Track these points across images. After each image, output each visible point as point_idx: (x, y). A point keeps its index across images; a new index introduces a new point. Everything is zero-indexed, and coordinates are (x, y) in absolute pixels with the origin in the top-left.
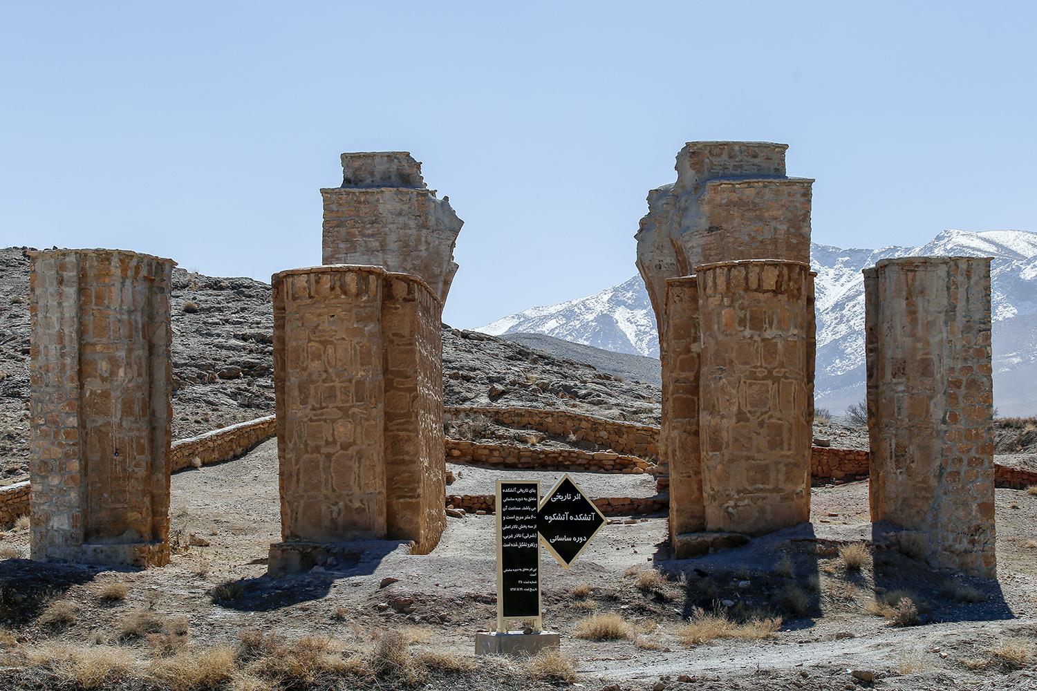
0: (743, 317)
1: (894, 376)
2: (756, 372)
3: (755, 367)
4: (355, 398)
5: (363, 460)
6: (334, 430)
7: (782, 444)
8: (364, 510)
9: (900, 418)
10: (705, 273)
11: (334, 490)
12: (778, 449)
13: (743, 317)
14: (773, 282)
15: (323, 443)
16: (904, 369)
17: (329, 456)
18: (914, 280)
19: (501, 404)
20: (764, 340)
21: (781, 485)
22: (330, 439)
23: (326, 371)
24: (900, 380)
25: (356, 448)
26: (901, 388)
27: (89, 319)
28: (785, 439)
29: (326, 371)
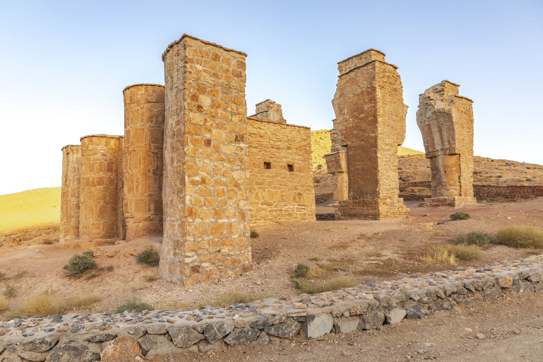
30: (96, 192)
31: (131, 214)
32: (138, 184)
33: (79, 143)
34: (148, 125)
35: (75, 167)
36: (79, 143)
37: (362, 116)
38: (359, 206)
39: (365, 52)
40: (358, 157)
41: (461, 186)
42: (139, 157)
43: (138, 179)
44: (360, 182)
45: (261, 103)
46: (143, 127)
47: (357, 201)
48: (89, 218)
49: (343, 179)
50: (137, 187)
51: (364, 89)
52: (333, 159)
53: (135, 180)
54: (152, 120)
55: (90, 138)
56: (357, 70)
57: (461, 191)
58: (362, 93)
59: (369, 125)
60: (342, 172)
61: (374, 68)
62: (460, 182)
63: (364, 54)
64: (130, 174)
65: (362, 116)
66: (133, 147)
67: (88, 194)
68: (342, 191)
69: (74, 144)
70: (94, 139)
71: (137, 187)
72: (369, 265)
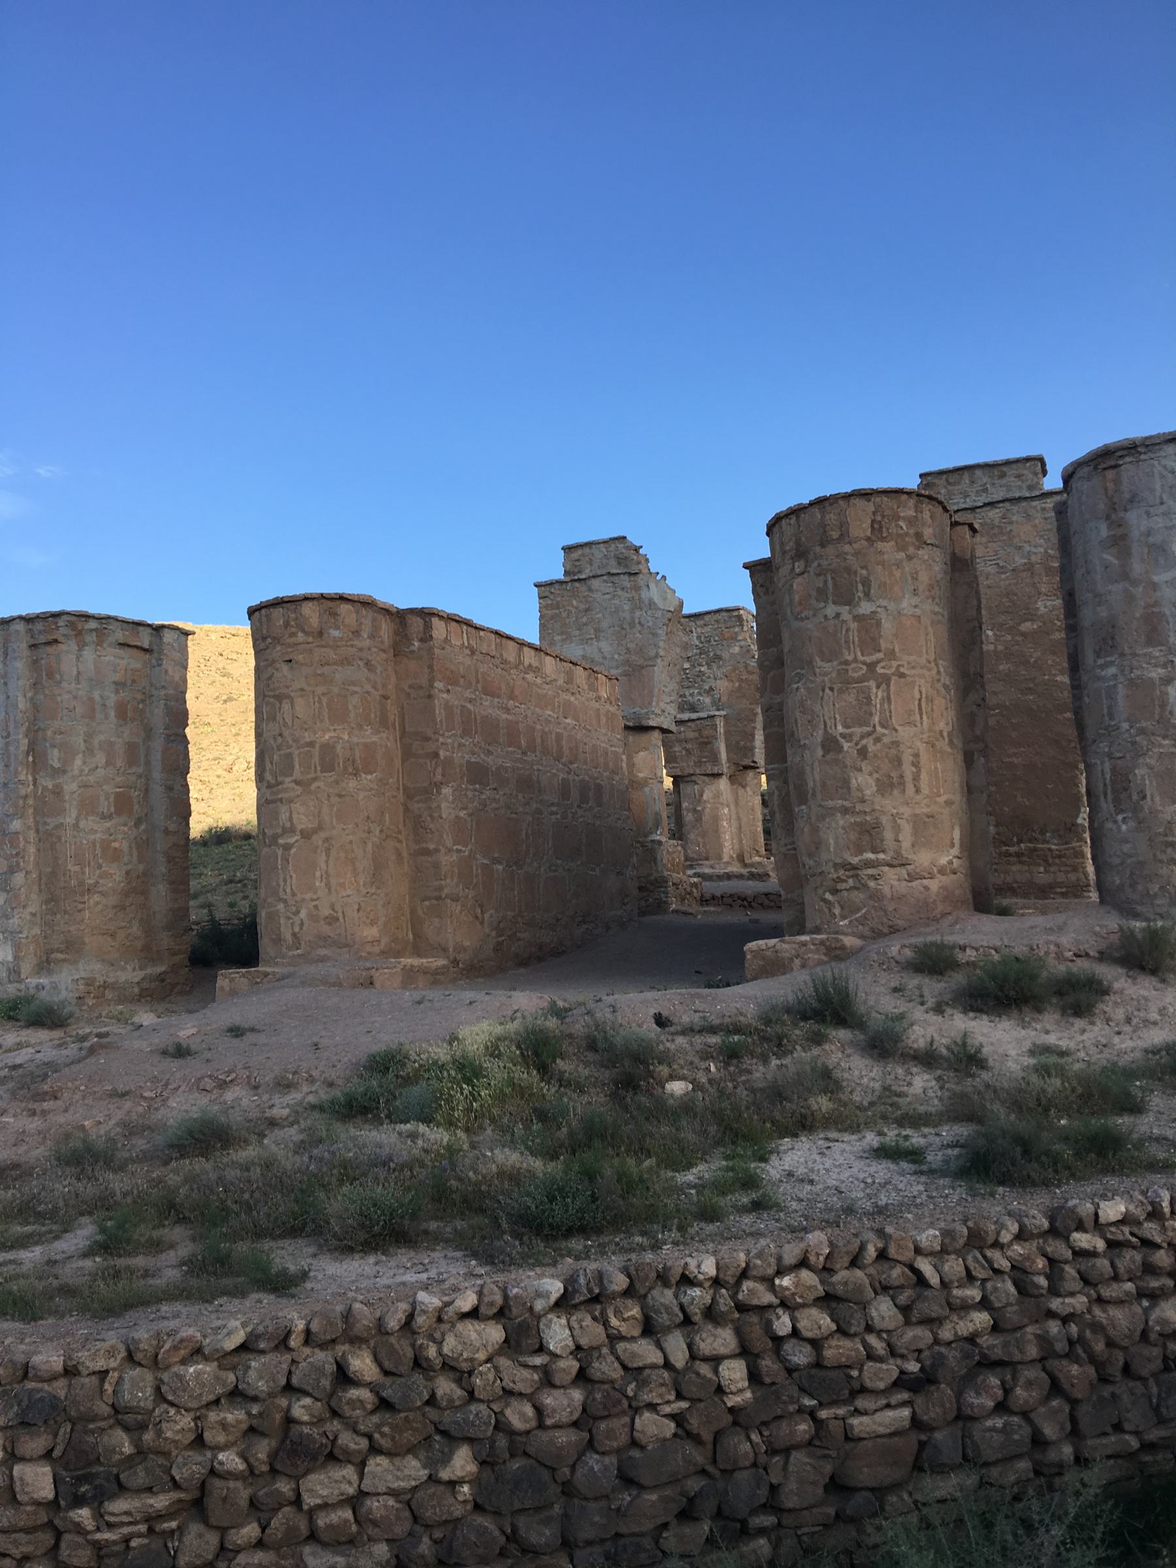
0: (821, 585)
1: (1098, 654)
2: (847, 671)
3: (846, 663)
4: (319, 768)
5: (333, 853)
6: (291, 813)
7: (902, 783)
8: (337, 919)
9: (1113, 723)
10: (798, 517)
11: (294, 895)
12: (896, 792)
13: (821, 585)
14: (867, 524)
15: (279, 831)
16: (1113, 638)
17: (287, 848)
18: (1117, 481)
19: (760, 756)
20: (857, 618)
21: (907, 853)
22: (288, 825)
23: (281, 735)
24: (1108, 659)
25: (323, 835)
26: (1112, 670)
27: (707, 618)
28: (908, 776)
29: (281, 735)
30: (362, 795)
31: (898, 853)
32: (919, 771)
35: (91, 700)
37: (1026, 626)
38: (1021, 863)
39: (1017, 461)
40: (1014, 734)
42: (917, 696)
43: (917, 755)
44: (1019, 799)
45: (589, 544)
46: (918, 612)
47: (1012, 849)
48: (342, 885)
49: (718, 795)
50: (916, 778)
52: (691, 735)
53: (907, 758)
54: (933, 593)
55: (330, 604)
56: (1007, 504)
58: (1029, 567)
59: (1054, 653)
60: (719, 775)
63: (1014, 466)
64: (886, 740)
65: (1026, 626)
66: (895, 664)
67: (334, 799)
68: (717, 831)
69: (92, 610)
70: (344, 608)
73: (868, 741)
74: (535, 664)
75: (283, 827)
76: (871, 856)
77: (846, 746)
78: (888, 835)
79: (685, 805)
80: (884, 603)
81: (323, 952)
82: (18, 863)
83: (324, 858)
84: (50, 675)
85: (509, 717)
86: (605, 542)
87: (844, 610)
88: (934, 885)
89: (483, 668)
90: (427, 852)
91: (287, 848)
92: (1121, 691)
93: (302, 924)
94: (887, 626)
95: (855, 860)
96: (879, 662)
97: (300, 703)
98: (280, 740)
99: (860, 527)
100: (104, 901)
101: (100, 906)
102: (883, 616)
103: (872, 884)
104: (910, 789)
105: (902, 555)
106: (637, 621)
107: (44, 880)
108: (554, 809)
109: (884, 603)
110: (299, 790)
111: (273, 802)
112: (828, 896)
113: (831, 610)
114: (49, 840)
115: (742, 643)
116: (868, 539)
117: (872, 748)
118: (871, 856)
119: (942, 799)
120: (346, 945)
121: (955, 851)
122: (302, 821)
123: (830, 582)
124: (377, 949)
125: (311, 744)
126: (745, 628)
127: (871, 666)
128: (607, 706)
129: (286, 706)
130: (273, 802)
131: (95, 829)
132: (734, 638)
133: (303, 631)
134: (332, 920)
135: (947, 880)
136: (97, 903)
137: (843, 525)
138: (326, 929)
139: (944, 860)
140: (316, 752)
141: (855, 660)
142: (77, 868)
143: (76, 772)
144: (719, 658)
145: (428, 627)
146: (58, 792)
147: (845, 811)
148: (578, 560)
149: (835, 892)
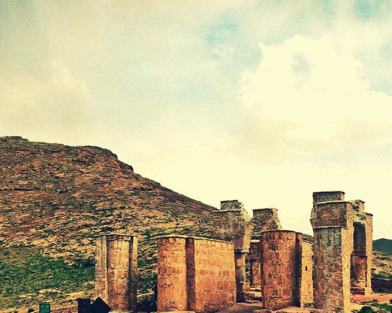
11: (166, 297)
17: (165, 288)
20: (276, 253)
21: (282, 296)
22: (165, 283)
23: (164, 265)
25: (172, 286)
28: (283, 282)
29: (164, 265)
31: (280, 296)
33: (218, 206)
34: (289, 251)
36: (218, 206)
41: (366, 280)
42: (285, 267)
45: (228, 201)
46: (286, 252)
50: (284, 283)
51: (338, 218)
53: (283, 279)
57: (366, 284)
61: (345, 206)
62: (366, 277)
71: (284, 283)
72: (224, 209)
73: (276, 276)
74: (214, 244)
75: (164, 284)
76: (276, 296)
77: (272, 276)
78: (279, 292)
79: (253, 268)
80: (280, 251)
81: (172, 309)
82: (105, 288)
83: (172, 290)
84: (112, 247)
85: (209, 258)
86: (232, 201)
87: (273, 251)
88: (286, 301)
89: (203, 248)
90: (191, 289)
91: (165, 288)
92: (317, 270)
93: (168, 303)
94: (280, 255)
95: (273, 297)
96: (279, 261)
97: (168, 258)
98: (164, 266)
99: (277, 236)
100: (122, 296)
101: (121, 298)
102: (280, 252)
103: (276, 301)
104: (283, 284)
105: (284, 242)
106: (239, 224)
107: (109, 292)
108: (217, 278)
109: (280, 251)
110: (168, 276)
111: (162, 278)
112: (268, 303)
113: (271, 251)
114: (110, 283)
115: (272, 220)
116: (278, 239)
117: (277, 277)
118: (276, 296)
119: (289, 286)
120: (176, 308)
121: (291, 295)
122: (168, 283)
123: (271, 246)
124: (182, 309)
125: (170, 267)
126: (274, 215)
127: (277, 262)
128: (231, 251)
129: (165, 259)
130: (162, 278)
131: (120, 281)
132: (270, 217)
133: (169, 244)
134: (174, 303)
135: (289, 301)
136: (121, 297)
137: (274, 236)
138: (172, 305)
139: (289, 297)
140: (171, 269)
141: (275, 261)
142: (117, 289)
143: (117, 269)
144: (266, 223)
145: (193, 241)
146: (113, 273)
147: (271, 288)
148: (224, 205)
149: (269, 302)
